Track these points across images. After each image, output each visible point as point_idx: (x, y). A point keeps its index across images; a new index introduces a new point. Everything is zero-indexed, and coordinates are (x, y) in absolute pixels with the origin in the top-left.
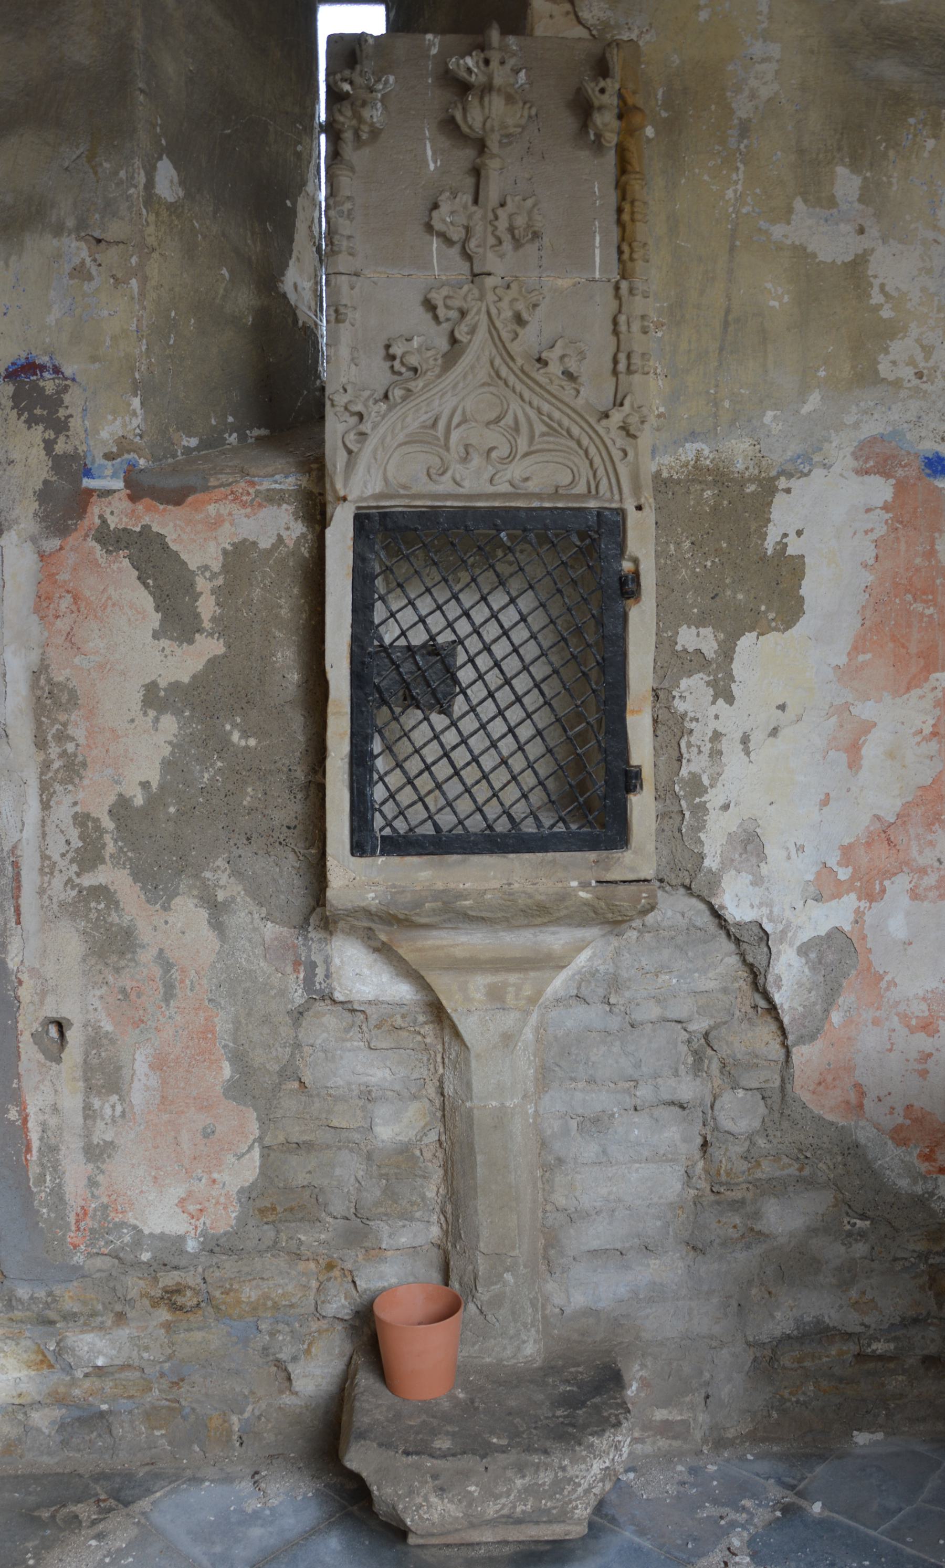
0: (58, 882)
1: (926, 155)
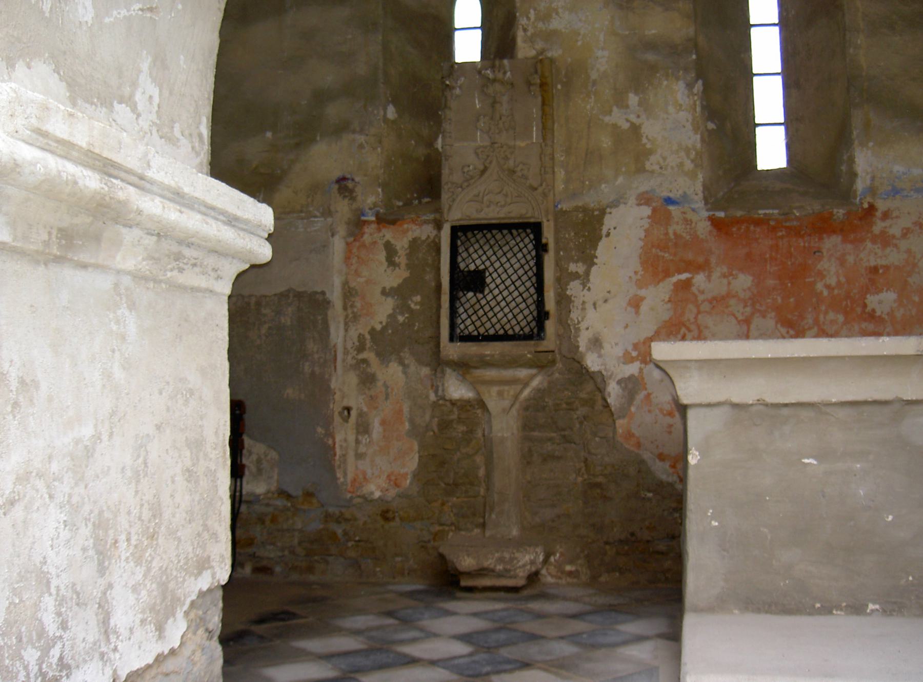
0: (349, 357)
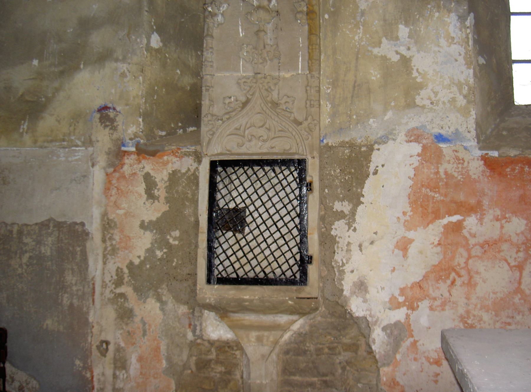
0: (108, 291)
1: (435, 19)
